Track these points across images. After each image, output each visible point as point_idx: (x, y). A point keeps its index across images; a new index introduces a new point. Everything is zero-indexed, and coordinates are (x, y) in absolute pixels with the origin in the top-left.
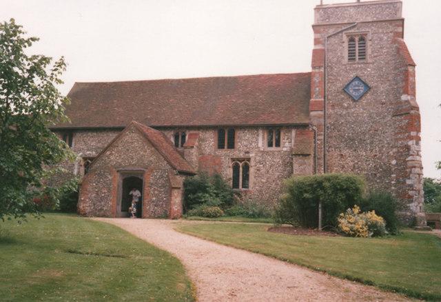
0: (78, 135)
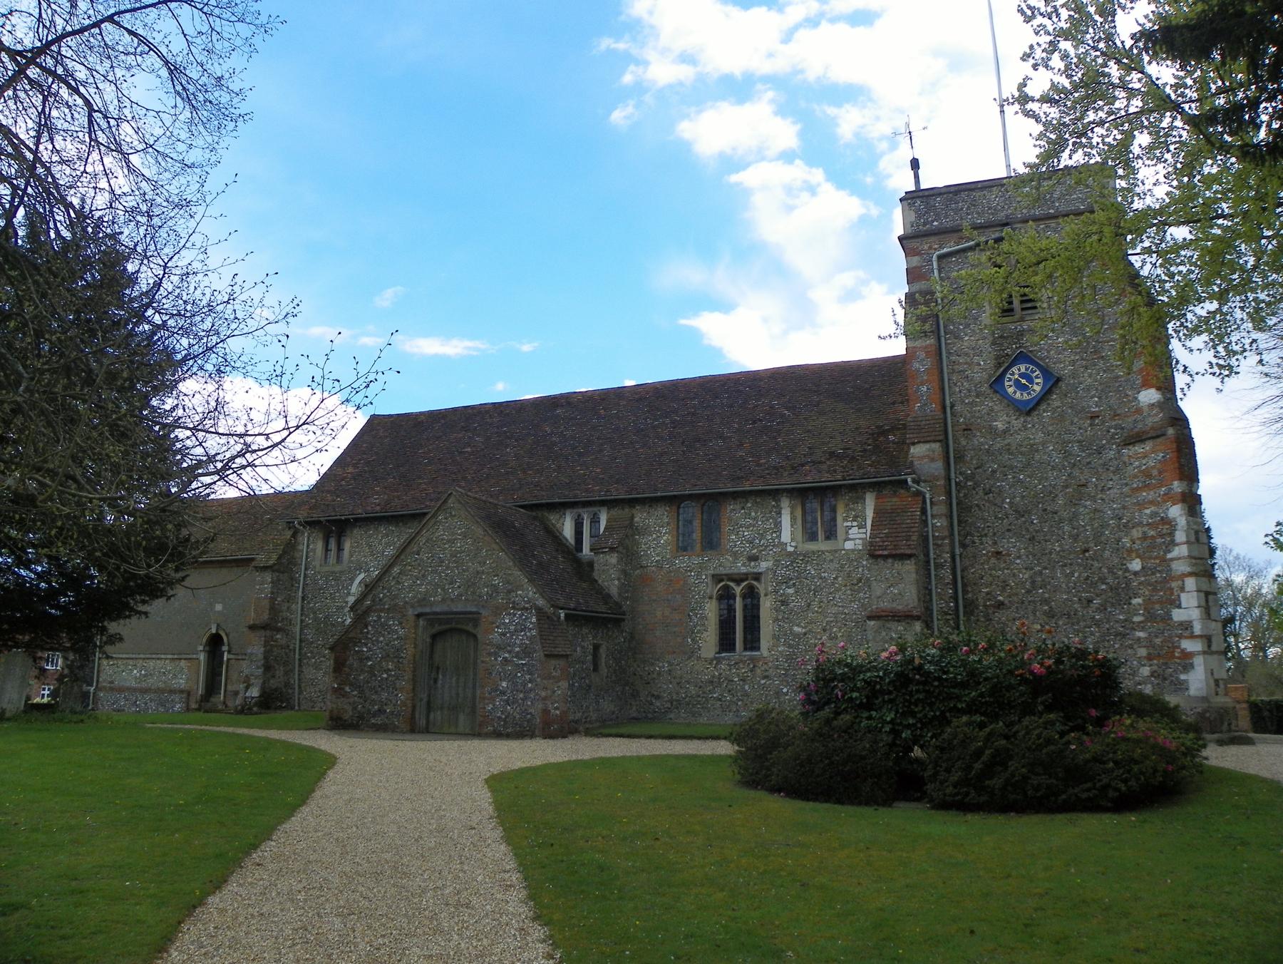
0: (357, 532)
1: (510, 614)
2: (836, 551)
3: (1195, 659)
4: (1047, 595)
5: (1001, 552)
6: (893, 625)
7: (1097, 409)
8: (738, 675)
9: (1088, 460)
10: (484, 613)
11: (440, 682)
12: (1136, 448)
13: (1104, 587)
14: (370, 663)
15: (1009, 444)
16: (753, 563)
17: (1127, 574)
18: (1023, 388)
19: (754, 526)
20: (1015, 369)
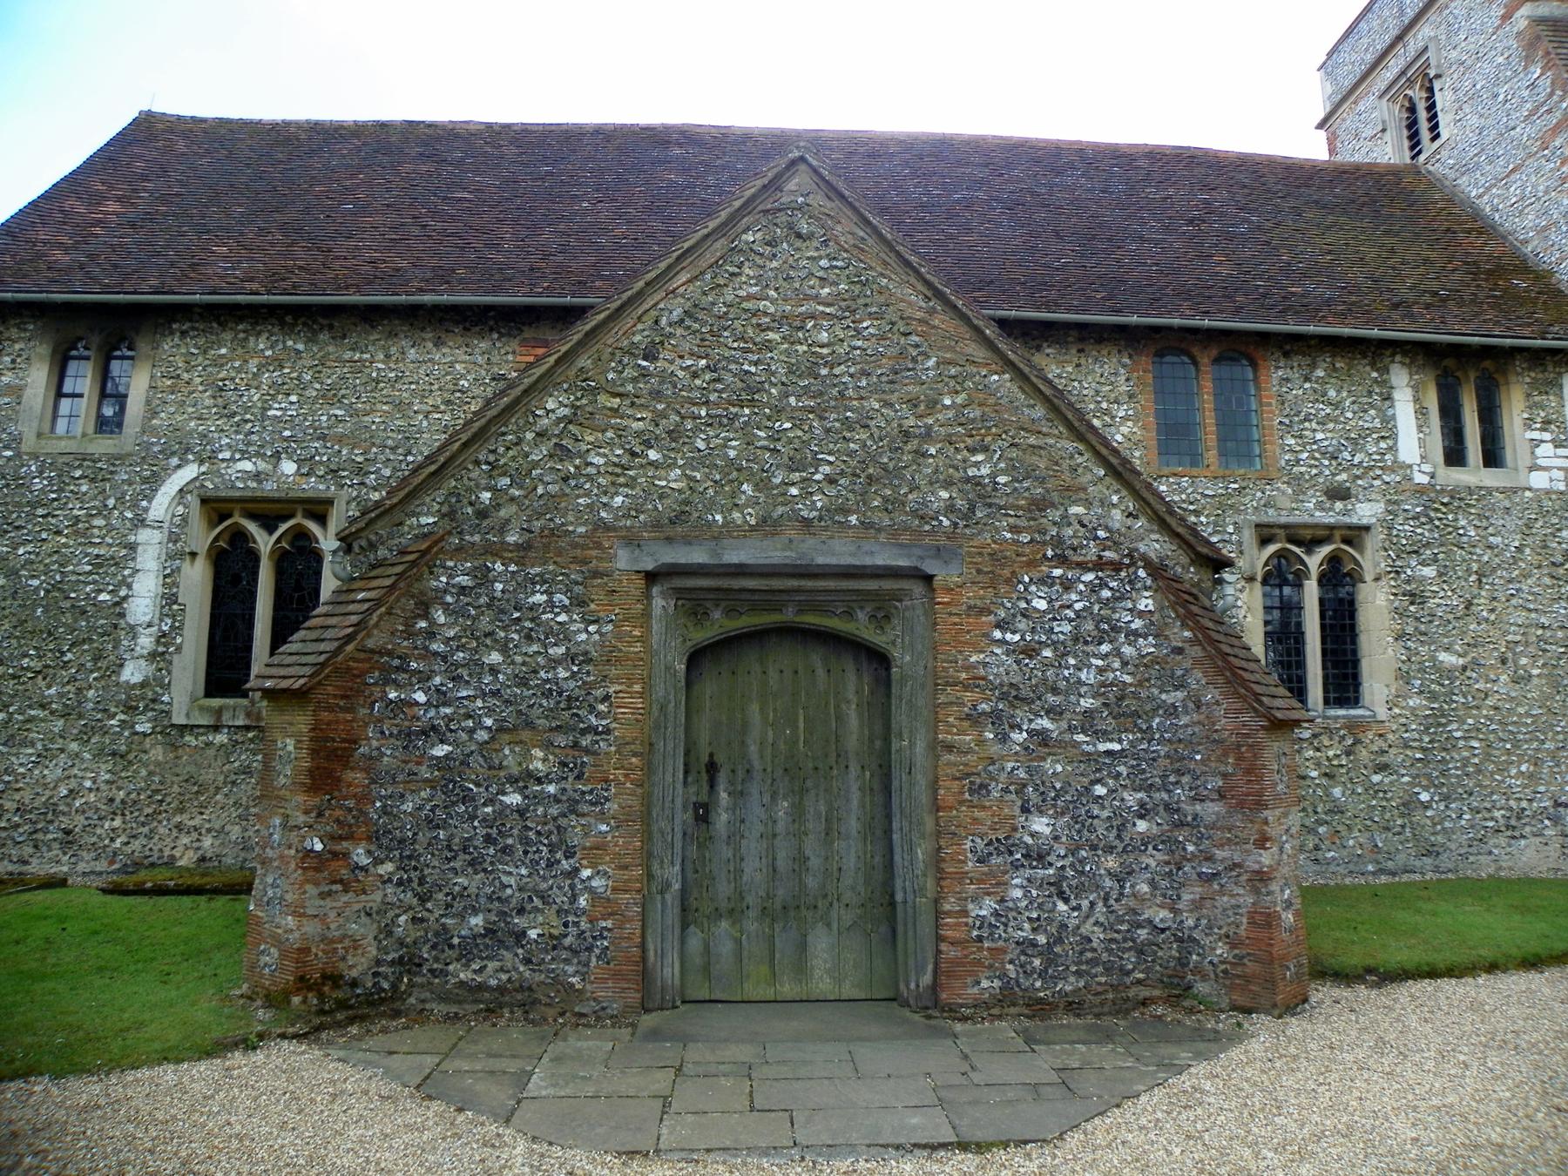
0: (174, 349)
1: (1048, 581)
2: (1514, 490)
8: (1318, 765)
10: (946, 574)
11: (723, 817)
14: (440, 751)
16: (1339, 505)
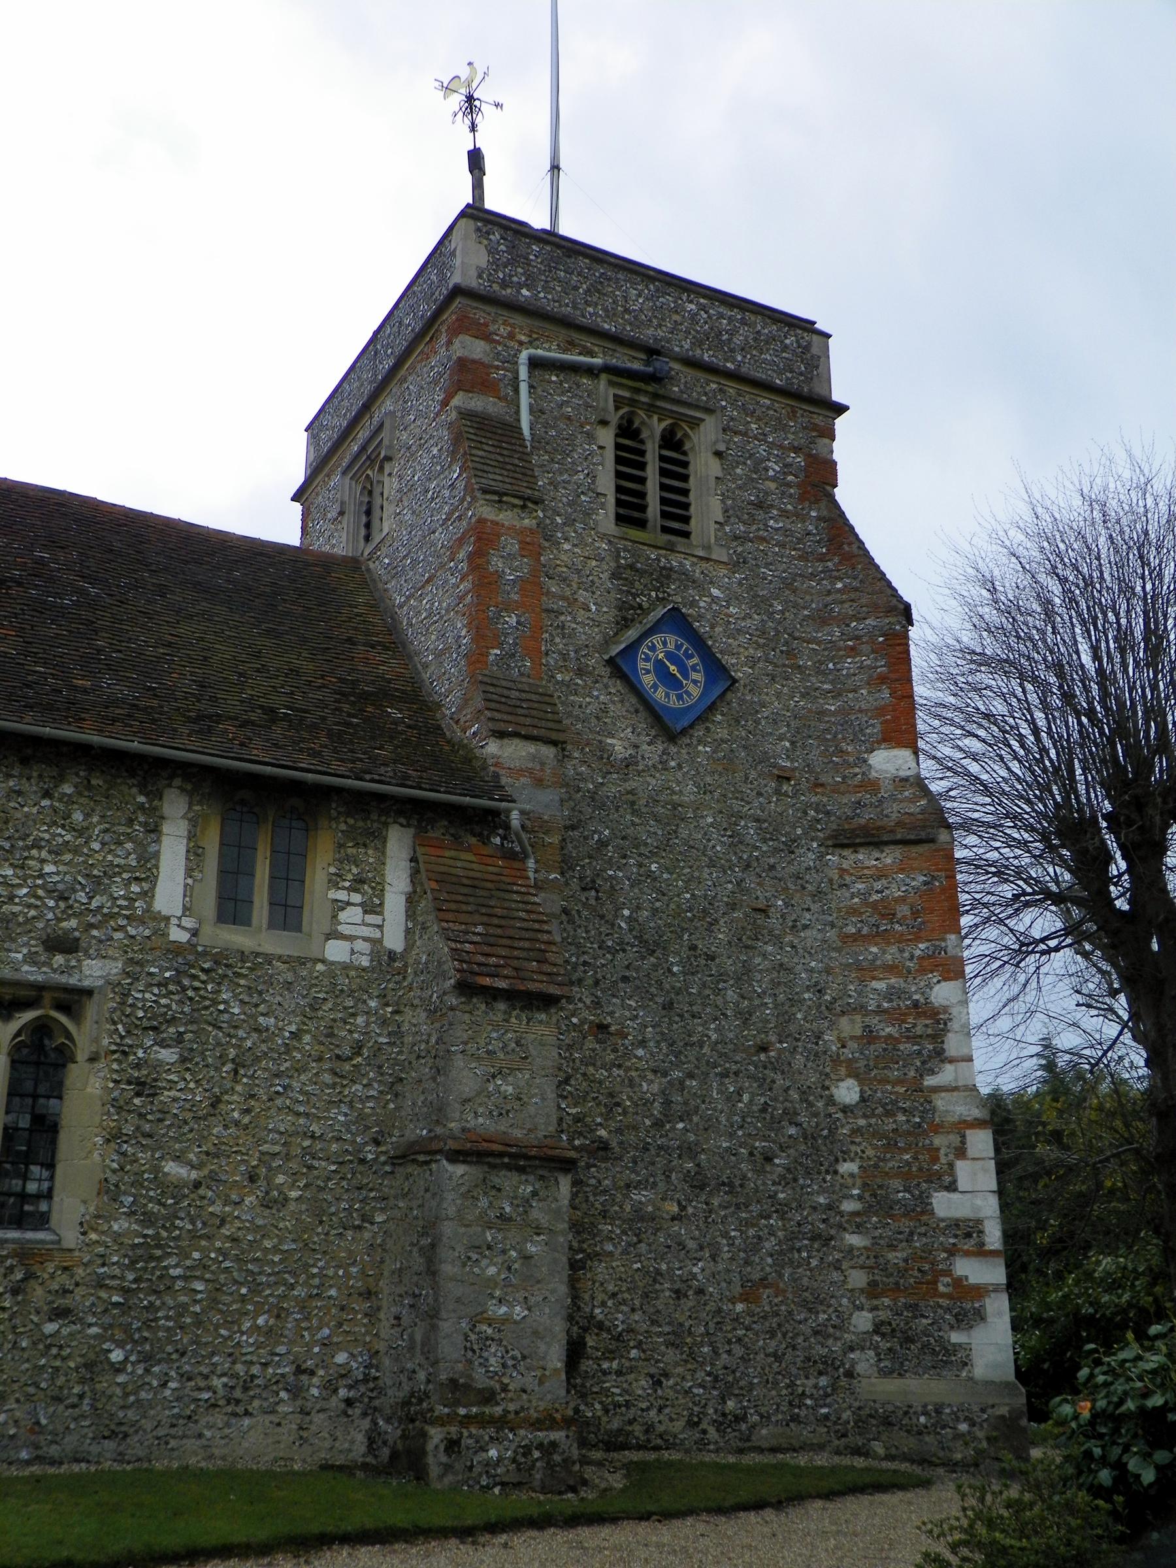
2: (302, 961)
3: (987, 1301)
4: (692, 1137)
5: (607, 1026)
6: (508, 1180)
7: (788, 764)
9: (772, 861)
12: (861, 857)
13: (792, 1131)
15: (631, 792)
16: (59, 959)
17: (832, 1110)
18: (671, 682)
19: (76, 851)
20: (656, 639)
